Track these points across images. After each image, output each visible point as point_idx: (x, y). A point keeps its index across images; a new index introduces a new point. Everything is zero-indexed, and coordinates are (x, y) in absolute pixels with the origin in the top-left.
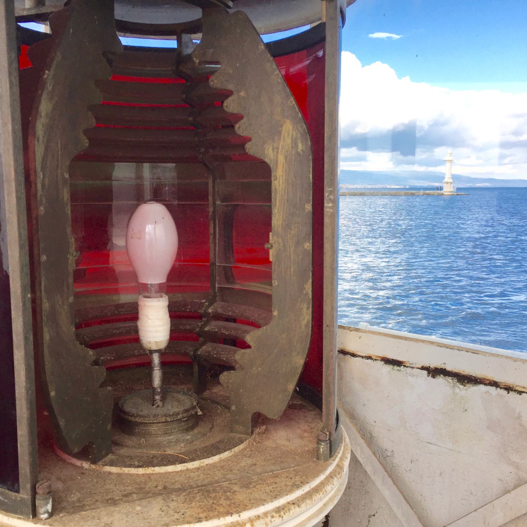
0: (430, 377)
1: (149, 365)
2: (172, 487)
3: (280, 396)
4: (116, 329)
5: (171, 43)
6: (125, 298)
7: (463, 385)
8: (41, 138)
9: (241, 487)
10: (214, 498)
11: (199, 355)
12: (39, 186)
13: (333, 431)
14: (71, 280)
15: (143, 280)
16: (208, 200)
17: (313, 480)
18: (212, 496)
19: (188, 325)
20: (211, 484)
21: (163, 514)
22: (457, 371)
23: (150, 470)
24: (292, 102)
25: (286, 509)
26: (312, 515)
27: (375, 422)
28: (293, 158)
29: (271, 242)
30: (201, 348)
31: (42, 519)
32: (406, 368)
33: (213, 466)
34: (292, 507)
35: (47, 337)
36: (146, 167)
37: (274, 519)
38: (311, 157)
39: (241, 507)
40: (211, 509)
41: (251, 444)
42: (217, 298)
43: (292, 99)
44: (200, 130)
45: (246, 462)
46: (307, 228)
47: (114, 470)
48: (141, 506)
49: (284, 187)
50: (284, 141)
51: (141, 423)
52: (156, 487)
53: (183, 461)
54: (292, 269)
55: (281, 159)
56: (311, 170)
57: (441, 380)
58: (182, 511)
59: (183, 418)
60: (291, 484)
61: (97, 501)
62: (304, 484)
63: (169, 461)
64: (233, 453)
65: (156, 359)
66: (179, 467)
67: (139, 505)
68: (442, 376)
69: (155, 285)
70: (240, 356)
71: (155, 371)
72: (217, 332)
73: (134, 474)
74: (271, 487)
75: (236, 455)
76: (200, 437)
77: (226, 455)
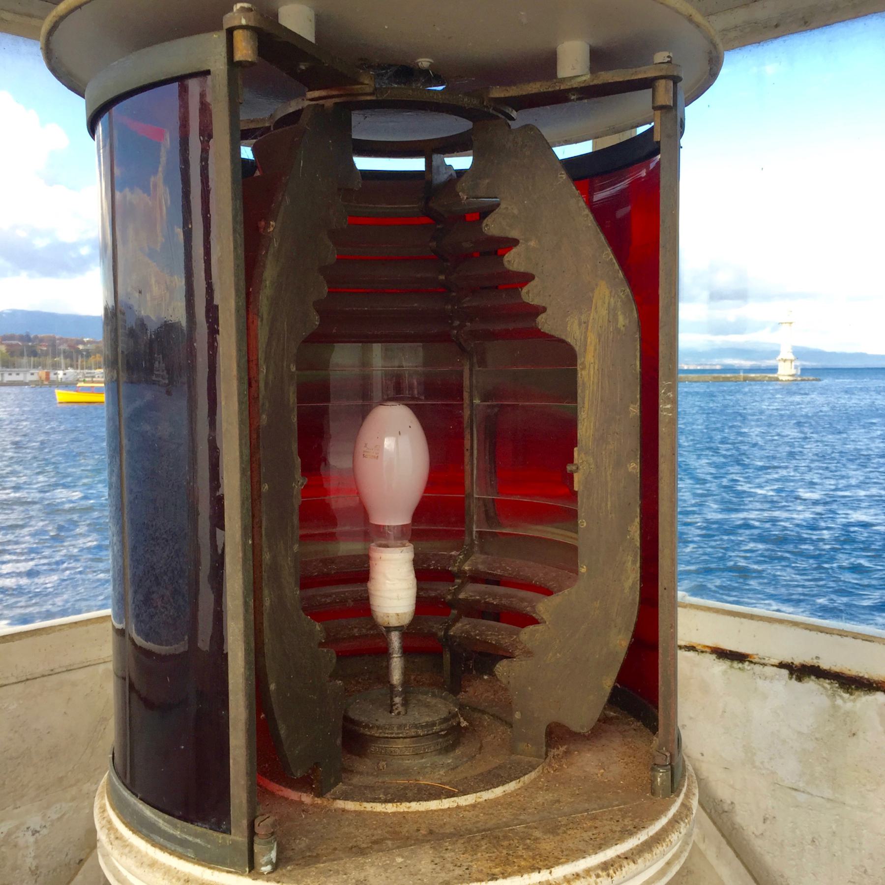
0: (793, 680)
1: (384, 652)
2: (442, 831)
3: (591, 697)
4: (326, 596)
5: (417, 164)
6: (347, 548)
7: (848, 692)
8: (265, 316)
9: (545, 833)
10: (509, 847)
11: (453, 636)
12: (262, 385)
13: (676, 752)
14: (296, 521)
15: (378, 519)
16: (462, 399)
17: (651, 824)
18: (508, 843)
19: (442, 589)
20: (498, 828)
21: (438, 868)
22: (838, 670)
23: (403, 807)
24: (608, 254)
25: (616, 865)
26: (650, 878)
27: (702, 755)
28: (611, 337)
29: (575, 462)
30: (453, 625)
31: (263, 874)
32: (752, 665)
33: (495, 802)
34: (625, 862)
35: (267, 603)
36: (377, 349)
37: (600, 879)
38: (637, 336)
39: (552, 860)
40: (507, 862)
41: (546, 772)
42: (476, 549)
43: (609, 250)
44: (454, 294)
45: (541, 798)
46: (633, 442)
47: (350, 806)
48: (403, 857)
49: (596, 380)
50: (596, 312)
51: (379, 737)
52: (418, 830)
53: (450, 795)
54: (609, 503)
55: (592, 338)
56: (638, 354)
57: (811, 685)
58: (465, 865)
59: (442, 730)
60: (619, 829)
61: (335, 849)
62: (639, 829)
63: (430, 794)
64: (521, 784)
65: (395, 640)
66: (447, 803)
67: (399, 855)
68: (813, 677)
69: (394, 527)
70: (526, 634)
71: (395, 659)
72: (478, 601)
73: (380, 813)
74: (590, 834)
75: (526, 788)
76: (467, 762)
77: (512, 786)
